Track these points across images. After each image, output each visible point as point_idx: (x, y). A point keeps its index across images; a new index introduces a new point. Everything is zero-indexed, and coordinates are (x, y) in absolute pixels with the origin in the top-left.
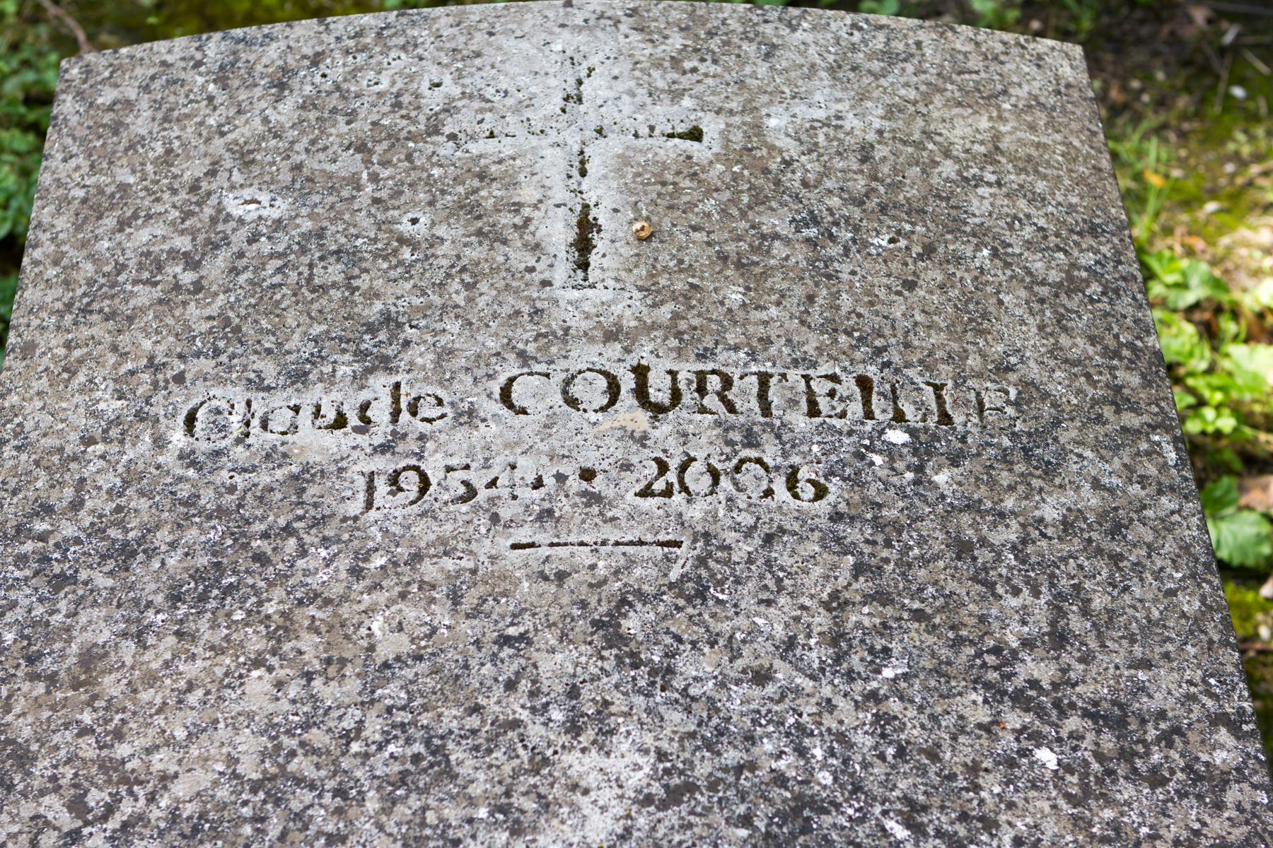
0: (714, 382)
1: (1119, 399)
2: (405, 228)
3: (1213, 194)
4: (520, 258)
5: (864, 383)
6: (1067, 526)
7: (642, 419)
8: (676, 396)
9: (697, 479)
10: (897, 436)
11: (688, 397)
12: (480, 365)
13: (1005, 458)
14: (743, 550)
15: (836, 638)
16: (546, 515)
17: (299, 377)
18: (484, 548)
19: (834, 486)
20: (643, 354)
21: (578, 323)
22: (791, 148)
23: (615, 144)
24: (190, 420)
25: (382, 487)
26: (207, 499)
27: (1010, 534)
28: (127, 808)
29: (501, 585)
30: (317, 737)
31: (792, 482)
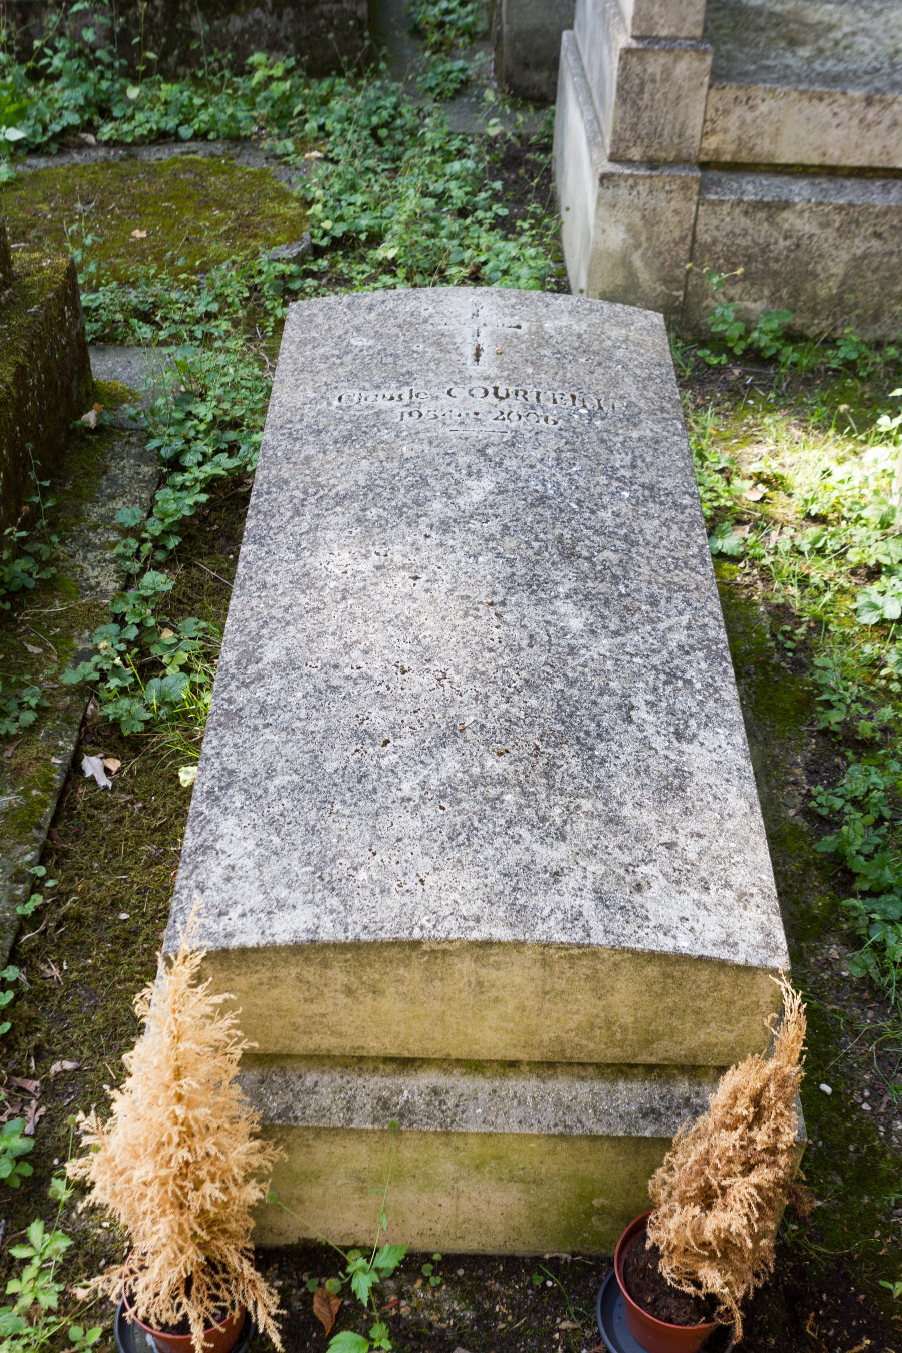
0: (521, 393)
1: (662, 410)
2: (415, 348)
3: (736, 437)
4: (454, 357)
5: (573, 397)
6: (640, 440)
7: (496, 401)
8: (508, 395)
9: (514, 417)
10: (584, 411)
11: (512, 396)
12: (440, 385)
13: (620, 420)
14: (529, 435)
15: (558, 459)
16: (462, 423)
17: (378, 387)
18: (441, 431)
19: (560, 422)
20: (497, 384)
21: (474, 374)
22: (553, 333)
23: (490, 328)
24: (340, 399)
25: (406, 416)
26: (346, 418)
27: (621, 439)
28: (321, 493)
29: (446, 440)
30: (384, 475)
31: (546, 420)
